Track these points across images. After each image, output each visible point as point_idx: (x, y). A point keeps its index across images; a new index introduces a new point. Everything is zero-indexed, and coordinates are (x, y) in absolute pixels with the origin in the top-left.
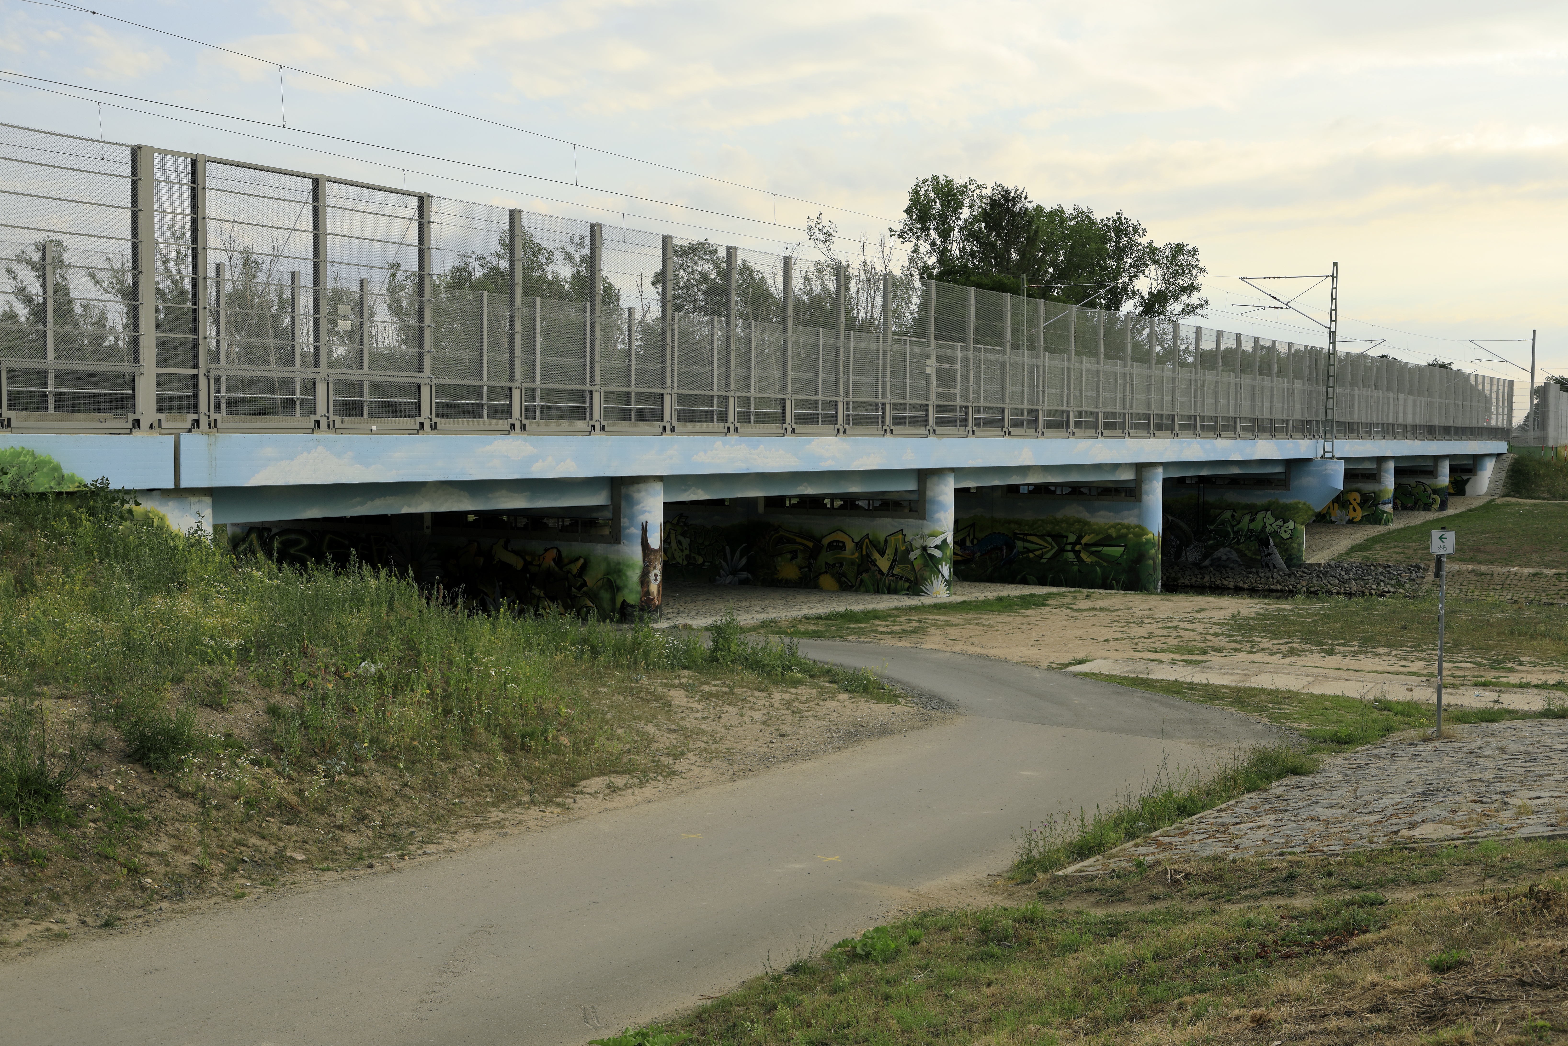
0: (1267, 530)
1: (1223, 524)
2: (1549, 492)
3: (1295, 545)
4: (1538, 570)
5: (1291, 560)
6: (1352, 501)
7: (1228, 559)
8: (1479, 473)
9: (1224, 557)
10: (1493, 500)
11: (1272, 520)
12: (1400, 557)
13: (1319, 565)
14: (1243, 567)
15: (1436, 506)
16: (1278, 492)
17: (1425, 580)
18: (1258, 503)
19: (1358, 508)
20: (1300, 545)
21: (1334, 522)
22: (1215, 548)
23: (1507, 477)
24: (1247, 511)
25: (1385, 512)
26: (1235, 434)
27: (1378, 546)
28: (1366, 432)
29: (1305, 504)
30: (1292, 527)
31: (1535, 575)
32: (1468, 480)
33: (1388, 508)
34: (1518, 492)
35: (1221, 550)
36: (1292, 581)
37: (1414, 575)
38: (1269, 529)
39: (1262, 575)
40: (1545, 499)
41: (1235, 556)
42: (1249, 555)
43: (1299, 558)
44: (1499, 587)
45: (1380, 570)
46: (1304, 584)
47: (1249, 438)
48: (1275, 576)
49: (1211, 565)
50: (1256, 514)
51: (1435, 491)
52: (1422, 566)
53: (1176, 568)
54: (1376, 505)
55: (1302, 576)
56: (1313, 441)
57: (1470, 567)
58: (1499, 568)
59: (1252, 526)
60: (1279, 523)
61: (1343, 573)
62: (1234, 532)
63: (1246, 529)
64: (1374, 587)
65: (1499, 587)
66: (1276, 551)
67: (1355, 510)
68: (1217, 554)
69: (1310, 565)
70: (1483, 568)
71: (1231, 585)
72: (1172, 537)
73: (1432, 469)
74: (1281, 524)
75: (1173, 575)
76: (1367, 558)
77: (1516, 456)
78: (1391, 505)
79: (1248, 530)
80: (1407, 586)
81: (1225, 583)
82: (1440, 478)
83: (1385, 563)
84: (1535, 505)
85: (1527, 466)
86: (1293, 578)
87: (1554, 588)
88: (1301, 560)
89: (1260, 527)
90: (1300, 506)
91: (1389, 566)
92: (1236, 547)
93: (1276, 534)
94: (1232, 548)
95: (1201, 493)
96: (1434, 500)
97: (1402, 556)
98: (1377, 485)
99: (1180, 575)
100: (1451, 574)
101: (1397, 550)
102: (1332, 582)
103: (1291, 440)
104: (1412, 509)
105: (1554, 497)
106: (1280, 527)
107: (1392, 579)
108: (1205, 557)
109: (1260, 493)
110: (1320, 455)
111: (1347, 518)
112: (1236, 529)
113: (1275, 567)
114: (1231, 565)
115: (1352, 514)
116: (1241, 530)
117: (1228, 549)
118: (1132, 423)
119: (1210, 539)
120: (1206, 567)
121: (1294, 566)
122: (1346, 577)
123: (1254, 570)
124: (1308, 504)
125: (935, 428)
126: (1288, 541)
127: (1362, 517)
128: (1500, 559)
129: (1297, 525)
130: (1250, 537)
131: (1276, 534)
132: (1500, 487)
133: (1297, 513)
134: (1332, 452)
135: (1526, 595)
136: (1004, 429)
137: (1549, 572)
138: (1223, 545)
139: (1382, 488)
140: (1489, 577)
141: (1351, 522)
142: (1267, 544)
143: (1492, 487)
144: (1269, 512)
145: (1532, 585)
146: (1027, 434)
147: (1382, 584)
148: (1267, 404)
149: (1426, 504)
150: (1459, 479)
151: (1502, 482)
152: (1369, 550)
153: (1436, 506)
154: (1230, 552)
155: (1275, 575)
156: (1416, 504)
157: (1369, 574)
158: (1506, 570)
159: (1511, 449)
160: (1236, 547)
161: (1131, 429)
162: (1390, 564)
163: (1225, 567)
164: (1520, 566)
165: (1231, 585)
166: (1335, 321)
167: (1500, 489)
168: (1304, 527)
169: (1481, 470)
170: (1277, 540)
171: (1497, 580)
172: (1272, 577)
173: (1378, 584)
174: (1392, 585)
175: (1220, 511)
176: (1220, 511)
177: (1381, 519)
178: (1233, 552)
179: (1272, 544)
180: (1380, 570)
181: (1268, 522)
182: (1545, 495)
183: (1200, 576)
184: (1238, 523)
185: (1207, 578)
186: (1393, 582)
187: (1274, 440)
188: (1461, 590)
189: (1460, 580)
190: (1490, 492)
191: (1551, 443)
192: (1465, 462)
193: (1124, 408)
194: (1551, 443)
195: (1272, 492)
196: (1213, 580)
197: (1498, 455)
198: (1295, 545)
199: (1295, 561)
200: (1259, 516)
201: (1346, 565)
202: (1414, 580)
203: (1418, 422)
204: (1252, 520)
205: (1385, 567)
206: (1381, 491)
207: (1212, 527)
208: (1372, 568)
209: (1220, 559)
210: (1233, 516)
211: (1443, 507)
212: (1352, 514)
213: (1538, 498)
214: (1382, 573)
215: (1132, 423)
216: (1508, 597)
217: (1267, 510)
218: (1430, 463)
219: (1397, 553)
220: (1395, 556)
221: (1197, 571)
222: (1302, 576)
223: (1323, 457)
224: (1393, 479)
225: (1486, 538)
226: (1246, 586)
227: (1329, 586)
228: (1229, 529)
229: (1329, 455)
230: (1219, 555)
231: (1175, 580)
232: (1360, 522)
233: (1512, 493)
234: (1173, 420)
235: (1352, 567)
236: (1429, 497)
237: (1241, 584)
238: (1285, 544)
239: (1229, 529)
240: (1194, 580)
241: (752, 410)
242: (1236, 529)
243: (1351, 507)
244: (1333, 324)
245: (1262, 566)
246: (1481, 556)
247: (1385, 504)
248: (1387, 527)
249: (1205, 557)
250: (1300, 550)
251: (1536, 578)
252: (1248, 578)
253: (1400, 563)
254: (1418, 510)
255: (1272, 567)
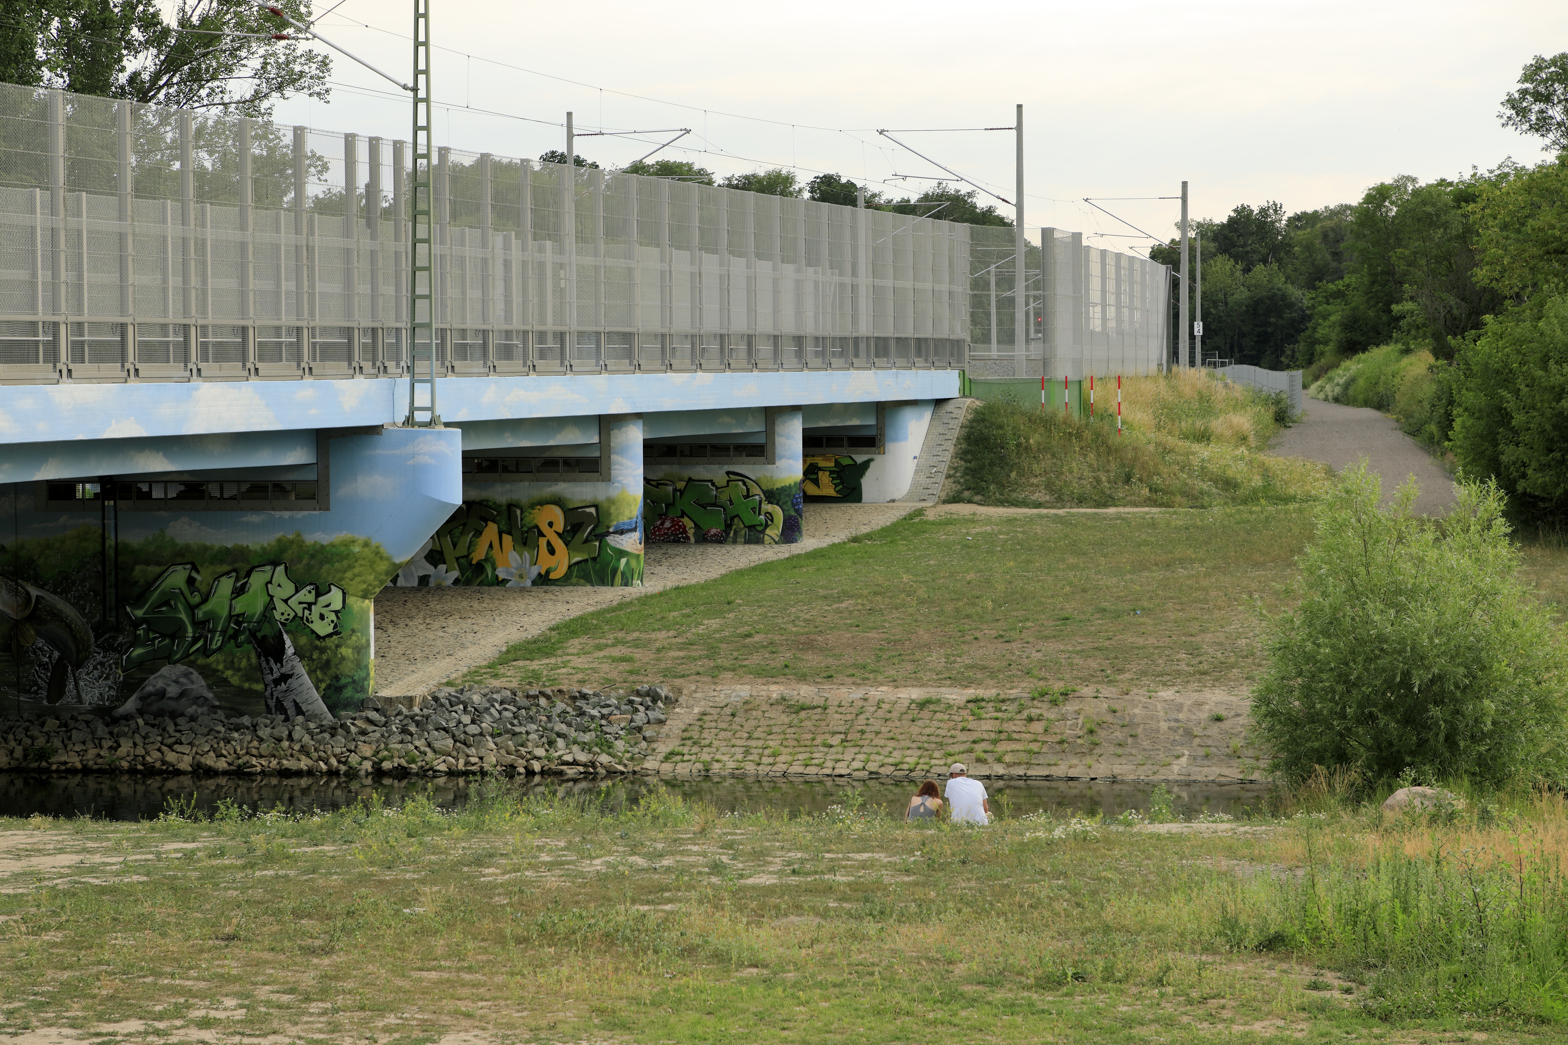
0: (277, 615)
1: (167, 603)
2: (1049, 487)
3: (346, 651)
4: (930, 692)
5: (340, 689)
6: (545, 528)
7: (183, 694)
8: (890, 447)
9: (173, 690)
10: (920, 512)
11: (289, 588)
12: (613, 672)
13: (410, 700)
14: (220, 714)
15: (774, 532)
16: (300, 514)
17: (665, 729)
18: (252, 547)
19: (559, 544)
20: (361, 650)
21: (504, 582)
22: (148, 665)
23: (956, 456)
24: (225, 568)
25: (622, 553)
26: (926, 361)
27: (574, 644)
28: (817, 354)
29: (366, 545)
30: (337, 605)
31: (923, 705)
32: (866, 465)
33: (632, 542)
34: (978, 490)
35: (165, 670)
36: (339, 745)
37: (640, 718)
38: (281, 612)
39: (263, 733)
40: (1038, 505)
41: (199, 685)
42: (235, 680)
43: (359, 685)
44: (836, 740)
45: (560, 706)
46: (367, 751)
47: (168, 379)
48: (296, 736)
49: (141, 712)
50: (248, 574)
51: (772, 496)
52: (663, 692)
53: (51, 723)
54: (601, 537)
55: (363, 733)
56: (383, 380)
57: (775, 691)
58: (844, 690)
59: (240, 606)
60: (305, 595)
61: (466, 719)
62: (196, 624)
63: (225, 613)
64: (540, 752)
65: (836, 740)
66: (301, 669)
67: (552, 551)
68: (154, 683)
69: (389, 701)
70: (805, 692)
71: (185, 764)
72: (40, 642)
73: (761, 440)
74: (311, 598)
75: (41, 742)
76: (536, 676)
77: (978, 403)
78: (637, 536)
79: (230, 616)
80: (620, 745)
81: (171, 757)
82: (781, 463)
83: (575, 688)
84: (1011, 521)
85: (1000, 427)
86: (340, 739)
87: (962, 736)
88: (363, 689)
89: (259, 608)
90: (356, 549)
91: (584, 697)
92: (201, 661)
93: (299, 624)
94: (192, 664)
95: (110, 523)
96: (770, 517)
97: (624, 666)
98: (601, 485)
99: (57, 743)
100: (728, 711)
101: (616, 652)
102: (437, 745)
103: (308, 381)
104: (720, 540)
105: (1060, 500)
106: (310, 605)
107: (587, 729)
108: (126, 689)
109: (255, 518)
110: (400, 419)
111: (535, 571)
112: (200, 614)
113: (299, 711)
114: (191, 710)
115: (546, 562)
116: (211, 617)
117: (181, 668)
118: (205, 345)
119: (135, 642)
120: (127, 717)
121: (347, 706)
122: (473, 729)
123: (246, 720)
124: (374, 543)
125: (71, 366)
126: (329, 642)
127: (570, 567)
128: (855, 665)
129: (351, 600)
130: (235, 635)
131: (299, 624)
132: (941, 478)
133: (350, 567)
134: (431, 409)
135: (897, 756)
136: (59, 366)
137: (956, 695)
138: (169, 659)
139: (613, 491)
140: (816, 714)
141: (543, 580)
142: (278, 653)
143: (923, 480)
144: (280, 569)
145: (915, 730)
146: (102, 374)
147: (560, 743)
148: (473, 294)
149: (751, 528)
150: (846, 462)
151: (944, 468)
152: (548, 655)
153: (774, 532)
154: (187, 675)
155: (298, 732)
156: (728, 526)
157: (531, 719)
158: (857, 694)
159: (968, 386)
160: (201, 661)
161: (261, 359)
162: (586, 690)
163: (174, 715)
164: (894, 682)
165: (185, 764)
166: (426, 72)
167: (941, 486)
168: (369, 605)
169: (896, 439)
170: (303, 641)
171: (836, 721)
172: (290, 738)
173: (551, 743)
174: (584, 746)
175: (158, 570)
176: (158, 570)
177: (615, 571)
178: (195, 675)
179: (290, 651)
180: (560, 706)
181: (279, 594)
182: (1038, 496)
183: (107, 744)
184: (205, 600)
185: (126, 747)
186: (587, 737)
187: (254, 382)
188: (747, 752)
189: (748, 726)
190: (918, 492)
191: (1062, 370)
192: (855, 422)
193: (186, 312)
194: (1062, 370)
195: (287, 514)
196: (140, 751)
197: (939, 403)
198: (346, 651)
199: (348, 693)
200: (257, 580)
201: (476, 698)
202: (639, 729)
203: (810, 329)
204: (239, 591)
205: (574, 698)
206: (611, 501)
207: (140, 613)
208: (543, 701)
209: (161, 694)
210: (191, 581)
211: (791, 532)
212: (546, 562)
213: (1024, 504)
214: (564, 713)
215: (205, 345)
216: (856, 764)
217: (275, 564)
218: (755, 426)
219: (614, 660)
220: (605, 667)
221: (101, 729)
222: (363, 733)
223: (409, 421)
224: (640, 471)
225: (839, 611)
226: (222, 764)
227: (430, 755)
228: (183, 616)
229: (421, 417)
230: (160, 684)
231: (43, 755)
232: (566, 581)
233: (967, 494)
234: (123, 335)
235: (492, 701)
236: (757, 510)
237: (210, 760)
238: (322, 650)
239: (183, 616)
240: (92, 752)
241: (40, 338)
242: (200, 614)
243: (543, 542)
244: (422, 78)
245: (269, 710)
246: (813, 660)
247: (622, 532)
248: (628, 589)
249: (126, 689)
250: (360, 664)
251: (925, 714)
252: (228, 741)
253: (610, 683)
254: (735, 542)
255: (291, 711)
